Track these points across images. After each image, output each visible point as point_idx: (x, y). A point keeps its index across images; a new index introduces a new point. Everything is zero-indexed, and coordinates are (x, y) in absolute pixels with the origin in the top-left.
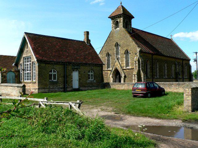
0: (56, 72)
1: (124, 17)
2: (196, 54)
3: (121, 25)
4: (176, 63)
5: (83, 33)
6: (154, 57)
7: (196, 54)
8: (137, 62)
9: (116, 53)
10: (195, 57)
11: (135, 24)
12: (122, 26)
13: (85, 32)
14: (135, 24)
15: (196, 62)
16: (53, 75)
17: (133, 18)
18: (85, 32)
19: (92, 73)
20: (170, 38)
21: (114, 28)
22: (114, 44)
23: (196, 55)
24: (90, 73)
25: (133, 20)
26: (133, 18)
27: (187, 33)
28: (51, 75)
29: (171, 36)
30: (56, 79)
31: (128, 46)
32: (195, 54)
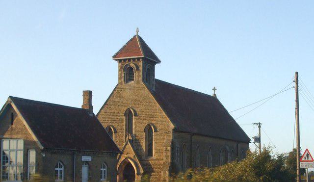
0: (63, 167)
1: (137, 60)
2: (260, 127)
3: (139, 76)
4: (228, 148)
5: (82, 94)
6: (195, 138)
7: (260, 127)
8: (169, 148)
9: (126, 128)
10: (256, 135)
11: (161, 73)
12: (141, 78)
13: (84, 92)
14: (161, 73)
15: (257, 144)
16: (59, 171)
17: (159, 62)
18: (84, 92)
19: (61, 169)
20: (211, 93)
21: (123, 80)
22: (124, 110)
23: (258, 129)
24: (103, 169)
25: (157, 66)
26: (159, 62)
27: (274, 155)
28: (57, 171)
29: (214, 89)
30: (63, 178)
31: (153, 117)
32: (257, 126)
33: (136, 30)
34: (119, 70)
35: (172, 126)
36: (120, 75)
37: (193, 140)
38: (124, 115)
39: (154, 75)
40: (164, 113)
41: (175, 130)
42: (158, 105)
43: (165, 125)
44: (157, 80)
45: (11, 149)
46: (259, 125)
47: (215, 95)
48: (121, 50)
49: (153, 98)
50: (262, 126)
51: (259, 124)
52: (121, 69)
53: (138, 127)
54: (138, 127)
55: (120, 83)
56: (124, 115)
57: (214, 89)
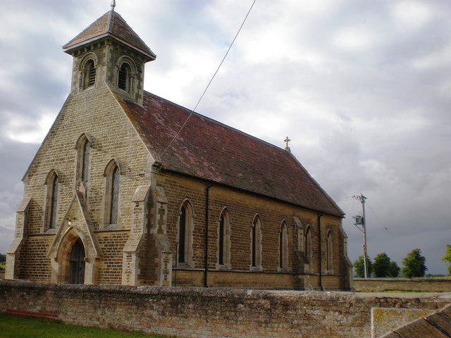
2: (363, 202)
4: (297, 220)
6: (214, 193)
7: (363, 202)
11: (157, 81)
14: (157, 81)
17: (150, 57)
20: (283, 146)
21: (78, 85)
22: (75, 138)
25: (148, 67)
26: (150, 57)
29: (287, 140)
30: (179, 289)
33: (110, 1)
34: (74, 70)
35: (151, 159)
36: (75, 77)
37: (211, 198)
38: (76, 148)
39: (141, 80)
40: (138, 136)
41: (156, 166)
42: (129, 121)
43: (141, 155)
44: (146, 93)
45: (202, 274)
46: (363, 198)
47: (287, 148)
48: (81, 34)
49: (122, 109)
50: (366, 200)
51: (363, 197)
52: (78, 67)
53: (97, 165)
54: (97, 165)
55: (74, 91)
56: (76, 148)
57: (287, 140)
